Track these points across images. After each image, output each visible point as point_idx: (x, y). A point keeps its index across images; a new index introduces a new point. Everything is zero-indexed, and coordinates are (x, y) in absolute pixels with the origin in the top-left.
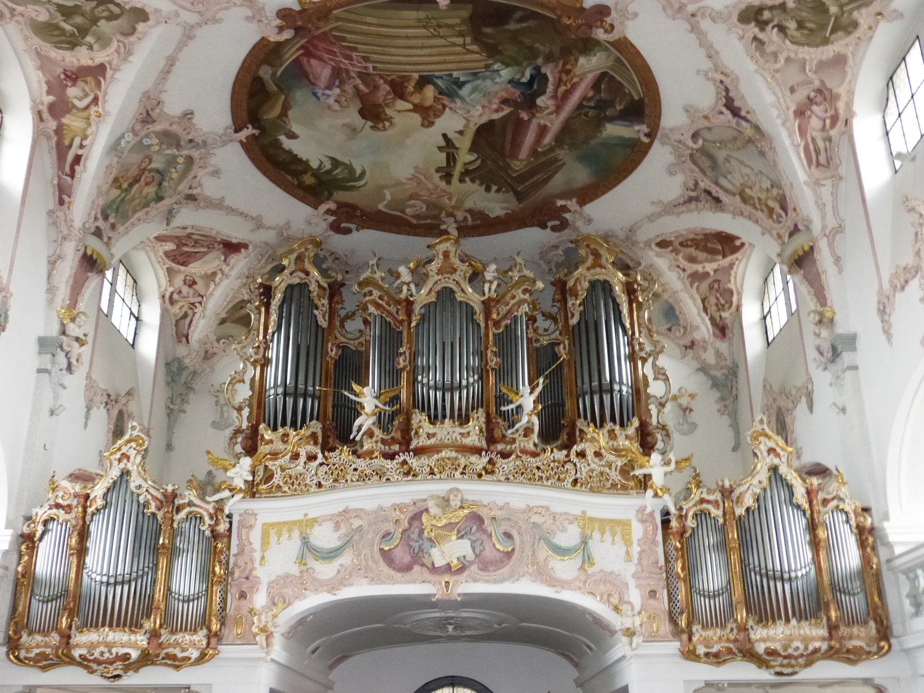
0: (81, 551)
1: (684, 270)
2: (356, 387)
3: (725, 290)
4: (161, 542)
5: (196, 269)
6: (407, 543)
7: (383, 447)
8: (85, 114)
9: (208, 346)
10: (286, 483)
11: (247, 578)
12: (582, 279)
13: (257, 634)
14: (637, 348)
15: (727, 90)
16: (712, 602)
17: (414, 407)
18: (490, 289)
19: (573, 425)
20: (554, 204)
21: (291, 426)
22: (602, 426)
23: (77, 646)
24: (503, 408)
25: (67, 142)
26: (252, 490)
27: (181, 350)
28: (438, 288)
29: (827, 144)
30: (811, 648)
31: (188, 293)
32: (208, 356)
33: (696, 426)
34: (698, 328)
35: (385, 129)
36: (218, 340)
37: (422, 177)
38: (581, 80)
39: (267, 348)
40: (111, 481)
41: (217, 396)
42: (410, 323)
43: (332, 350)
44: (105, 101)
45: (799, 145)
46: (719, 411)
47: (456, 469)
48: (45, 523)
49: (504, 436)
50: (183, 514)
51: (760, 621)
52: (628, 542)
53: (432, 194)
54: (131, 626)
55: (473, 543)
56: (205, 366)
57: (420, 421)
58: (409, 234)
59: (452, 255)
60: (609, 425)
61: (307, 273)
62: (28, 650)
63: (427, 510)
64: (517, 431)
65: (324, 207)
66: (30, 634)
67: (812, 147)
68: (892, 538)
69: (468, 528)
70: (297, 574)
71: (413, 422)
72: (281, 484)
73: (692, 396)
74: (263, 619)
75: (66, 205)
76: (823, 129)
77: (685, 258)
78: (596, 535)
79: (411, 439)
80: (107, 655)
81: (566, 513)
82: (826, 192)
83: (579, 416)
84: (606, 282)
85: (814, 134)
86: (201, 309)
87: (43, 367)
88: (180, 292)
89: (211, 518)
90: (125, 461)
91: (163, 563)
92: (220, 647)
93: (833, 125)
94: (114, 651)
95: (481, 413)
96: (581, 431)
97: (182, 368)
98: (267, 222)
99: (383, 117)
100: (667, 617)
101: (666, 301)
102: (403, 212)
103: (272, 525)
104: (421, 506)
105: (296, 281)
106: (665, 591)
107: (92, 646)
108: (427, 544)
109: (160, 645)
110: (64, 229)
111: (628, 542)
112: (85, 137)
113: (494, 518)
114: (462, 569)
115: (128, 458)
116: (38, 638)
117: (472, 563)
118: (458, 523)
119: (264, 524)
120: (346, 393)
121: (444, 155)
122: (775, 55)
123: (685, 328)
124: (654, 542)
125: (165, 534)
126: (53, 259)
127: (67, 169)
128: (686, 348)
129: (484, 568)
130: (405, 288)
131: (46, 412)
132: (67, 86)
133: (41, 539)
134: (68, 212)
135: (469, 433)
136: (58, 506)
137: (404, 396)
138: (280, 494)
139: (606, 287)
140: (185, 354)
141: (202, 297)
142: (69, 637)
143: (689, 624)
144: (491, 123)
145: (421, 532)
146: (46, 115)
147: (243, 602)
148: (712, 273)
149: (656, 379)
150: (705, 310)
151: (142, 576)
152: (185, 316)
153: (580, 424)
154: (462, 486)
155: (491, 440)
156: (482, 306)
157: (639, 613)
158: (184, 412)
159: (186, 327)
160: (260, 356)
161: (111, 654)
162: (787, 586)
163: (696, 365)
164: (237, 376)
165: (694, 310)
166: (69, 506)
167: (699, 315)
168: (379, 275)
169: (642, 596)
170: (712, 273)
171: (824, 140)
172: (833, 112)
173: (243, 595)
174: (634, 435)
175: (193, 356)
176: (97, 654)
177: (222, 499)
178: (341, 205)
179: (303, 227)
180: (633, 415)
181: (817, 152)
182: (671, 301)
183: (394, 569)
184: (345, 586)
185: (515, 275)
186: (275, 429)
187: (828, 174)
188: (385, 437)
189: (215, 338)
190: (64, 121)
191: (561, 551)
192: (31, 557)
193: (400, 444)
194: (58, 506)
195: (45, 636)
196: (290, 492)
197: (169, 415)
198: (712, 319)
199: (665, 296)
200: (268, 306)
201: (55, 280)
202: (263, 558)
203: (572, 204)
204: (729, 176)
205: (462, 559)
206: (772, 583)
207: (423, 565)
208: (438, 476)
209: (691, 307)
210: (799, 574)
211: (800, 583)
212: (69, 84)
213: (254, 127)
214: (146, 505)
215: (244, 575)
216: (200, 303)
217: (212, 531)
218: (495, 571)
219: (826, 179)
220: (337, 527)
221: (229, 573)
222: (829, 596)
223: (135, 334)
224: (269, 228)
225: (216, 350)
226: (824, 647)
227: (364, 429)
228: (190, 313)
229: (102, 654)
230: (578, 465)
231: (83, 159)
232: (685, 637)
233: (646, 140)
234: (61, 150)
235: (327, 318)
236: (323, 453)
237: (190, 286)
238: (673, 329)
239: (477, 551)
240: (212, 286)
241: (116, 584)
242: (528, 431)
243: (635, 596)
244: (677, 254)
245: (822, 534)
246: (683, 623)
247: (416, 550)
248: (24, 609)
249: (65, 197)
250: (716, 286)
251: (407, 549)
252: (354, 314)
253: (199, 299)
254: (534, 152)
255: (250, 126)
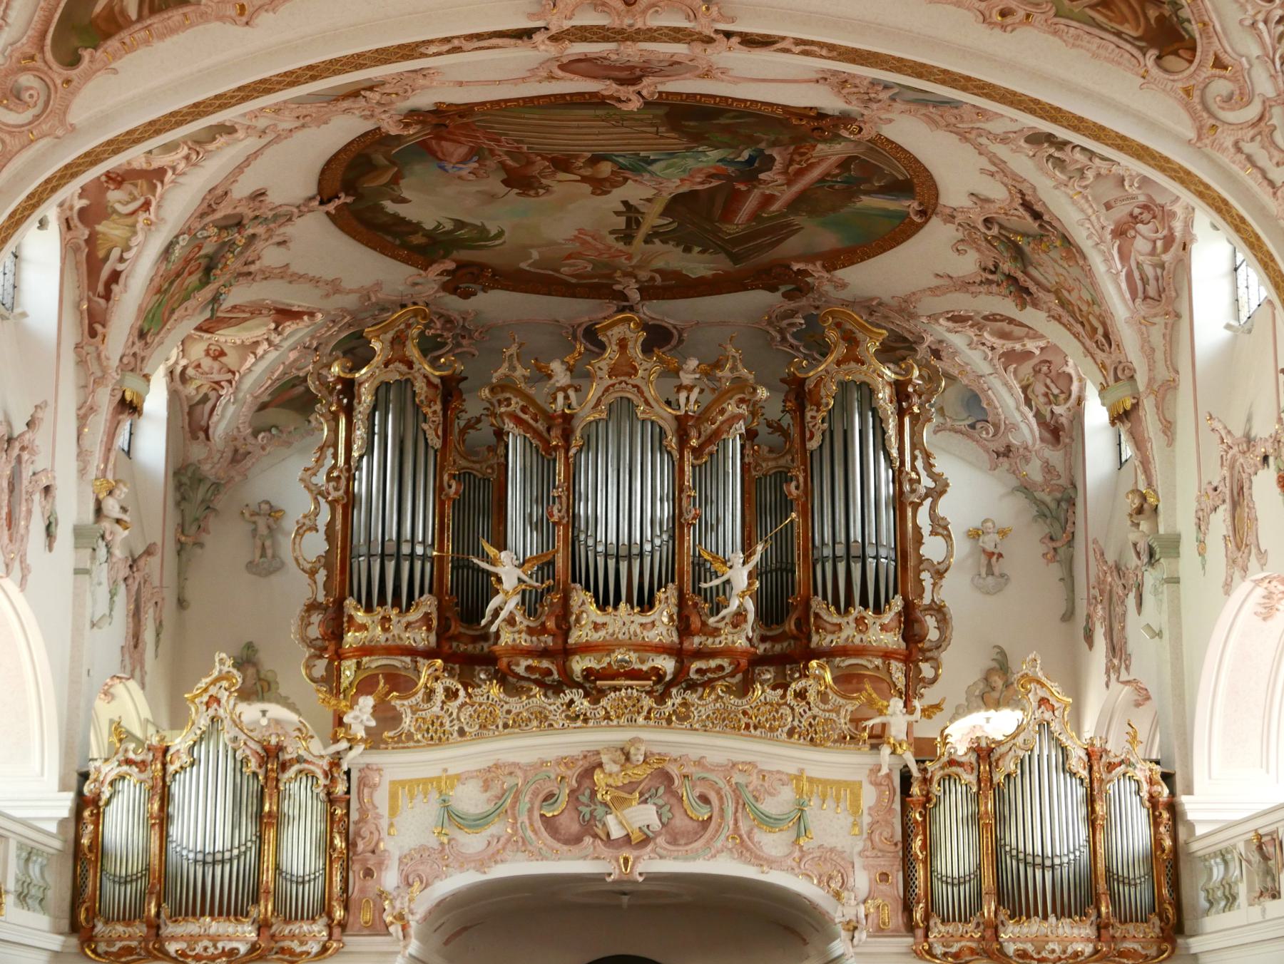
0: (163, 820)
1: (993, 348)
2: (492, 551)
3: (1059, 374)
4: (267, 808)
5: (228, 337)
6: (577, 802)
7: (528, 638)
8: (130, 220)
9: (238, 444)
10: (419, 729)
11: (373, 852)
12: (827, 379)
13: (392, 923)
14: (907, 487)
15: (1023, 195)
16: (956, 890)
17: (574, 581)
18: (688, 398)
19: (807, 606)
20: (788, 267)
21: (393, 606)
22: (847, 612)
23: (173, 938)
24: (703, 585)
25: (101, 254)
26: (374, 740)
27: (197, 451)
28: (611, 398)
29: (1159, 271)
30: (1070, 951)
31: (212, 368)
32: (238, 457)
33: (1008, 579)
34: (1015, 427)
35: (537, 195)
36: (255, 434)
37: (589, 239)
38: (818, 163)
39: (351, 478)
40: (199, 732)
41: (254, 523)
42: (567, 451)
43: (450, 487)
44: (159, 206)
45: (1118, 273)
46: (1044, 555)
47: (639, 713)
48: (112, 784)
49: (704, 624)
50: (291, 772)
51: (1011, 917)
52: (855, 809)
53: (601, 254)
54: (236, 915)
55: (659, 807)
56: (233, 473)
57: (583, 603)
58: (563, 296)
59: (630, 344)
60: (857, 610)
61: (410, 365)
62: (110, 942)
63: (600, 765)
64: (723, 618)
65: (436, 268)
66: (107, 922)
67: (1137, 275)
68: (1190, 816)
69: (653, 790)
70: (436, 846)
71: (572, 603)
72: (413, 730)
73: (1003, 533)
74: (398, 904)
75: (99, 338)
76: (1153, 252)
77: (993, 333)
78: (815, 802)
79: (569, 629)
80: (211, 950)
81: (778, 772)
82: (1156, 334)
83: (816, 593)
84: (863, 383)
85: (1141, 258)
86: (231, 390)
87: (81, 566)
88: (199, 366)
89: (326, 776)
90: (215, 705)
91: (270, 834)
92: (345, 939)
93: (1166, 248)
94: (220, 945)
95: (672, 590)
96: (817, 616)
97: (199, 480)
98: (348, 284)
99: (536, 185)
100: (900, 907)
101: (966, 386)
102: (558, 271)
103: (402, 783)
104: (593, 759)
105: (393, 376)
106: (901, 874)
107: (193, 939)
108: (600, 810)
109: (273, 936)
110: (94, 367)
111: (855, 809)
112: (127, 248)
113: (686, 777)
114: (646, 841)
115: (218, 701)
116: (120, 928)
117: (657, 834)
118: (641, 782)
119: (393, 783)
120: (476, 561)
121: (623, 219)
122: (1081, 171)
123: (997, 427)
124: (890, 810)
125: (271, 799)
126: (83, 411)
127: (101, 288)
128: (998, 455)
129: (674, 841)
130: (560, 396)
131: (88, 625)
132: (108, 188)
133: (108, 803)
134: (101, 347)
135: (653, 623)
136: (129, 762)
137: (560, 563)
138: (411, 744)
139: (867, 392)
140: (203, 456)
141: (234, 373)
142: (158, 927)
143: (927, 918)
144: (693, 193)
145: (594, 793)
146: (75, 221)
147: (370, 882)
148: (1037, 352)
149: (933, 533)
150: (1028, 402)
151: (245, 853)
152: (205, 399)
153: (817, 604)
154: (645, 735)
155: (684, 629)
156: (674, 425)
157: (865, 902)
158: (201, 545)
159: (206, 415)
160: (341, 492)
161: (216, 948)
162: (1048, 875)
163: (1014, 482)
164: (307, 522)
165: (1011, 402)
166: (143, 762)
167: (1018, 409)
168: (520, 372)
169: (870, 880)
170: (1037, 352)
171: (1155, 266)
172: (1165, 232)
173: (368, 873)
174: (894, 624)
175: (216, 460)
176: (199, 949)
177: (338, 753)
178: (461, 265)
179: (401, 288)
180: (895, 592)
181: (1145, 281)
182: (974, 387)
183: (559, 840)
184: (496, 862)
185: (725, 373)
186: (369, 609)
187: (1158, 310)
188: (532, 625)
189: (250, 430)
190: (99, 228)
191: (770, 822)
192: (97, 825)
193: (554, 635)
194: (129, 762)
195: (128, 925)
196: (424, 742)
197: (179, 553)
198: (1038, 415)
199: (965, 381)
200: (349, 411)
201: (86, 443)
202: (391, 825)
203: (816, 269)
204: (1041, 269)
205: (645, 829)
206: (1030, 870)
207: (596, 836)
208: (615, 723)
209: (1005, 397)
210: (1065, 860)
211: (1065, 871)
212: (112, 187)
213: (347, 195)
214: (245, 761)
215: (370, 848)
216: (230, 382)
217: (329, 794)
218: (686, 844)
219: (1155, 316)
220: (486, 786)
221: (350, 845)
222: (1102, 886)
223: (131, 434)
224: (351, 291)
225: (250, 448)
226: (1089, 949)
227: (503, 614)
228: (213, 395)
229: (206, 949)
230: (797, 709)
231: (123, 276)
232: (920, 933)
233: (917, 219)
234: (93, 264)
235: (440, 433)
236: (466, 689)
237: (215, 358)
238: (978, 426)
239: (665, 820)
240: (251, 359)
241: (214, 863)
242: (740, 615)
243: (861, 880)
244: (980, 329)
245: (1100, 809)
246: (918, 915)
247: (587, 818)
248: (94, 890)
249: (98, 327)
250: (1045, 369)
251: (575, 815)
252: (479, 420)
253: (229, 376)
254: (755, 216)
255: (342, 195)
